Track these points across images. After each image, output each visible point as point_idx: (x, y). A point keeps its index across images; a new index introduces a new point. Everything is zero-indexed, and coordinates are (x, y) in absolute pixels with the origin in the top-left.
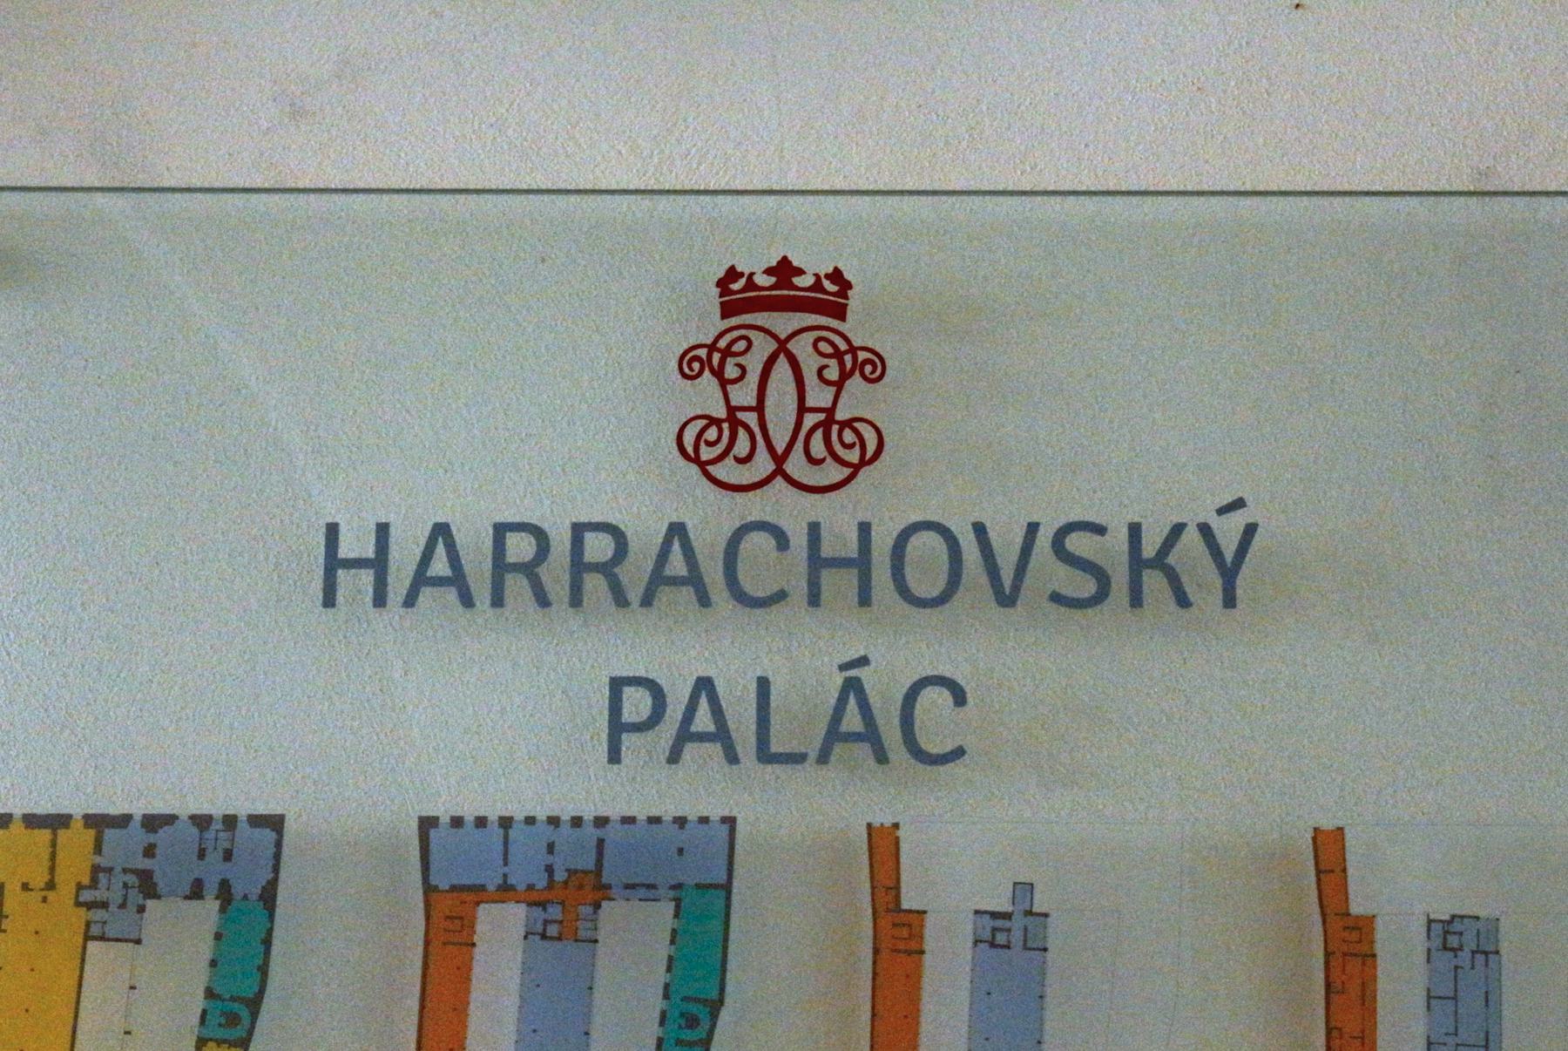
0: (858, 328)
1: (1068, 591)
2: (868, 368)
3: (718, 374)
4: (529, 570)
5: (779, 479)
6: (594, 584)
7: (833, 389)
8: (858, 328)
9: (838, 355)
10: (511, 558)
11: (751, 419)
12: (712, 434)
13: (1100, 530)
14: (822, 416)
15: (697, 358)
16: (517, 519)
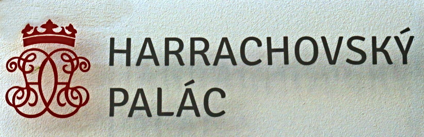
0: (78, 49)
1: (353, 59)
2: (83, 66)
3: (23, 69)
4: (176, 53)
5: (47, 113)
7: (69, 75)
9: (71, 60)
10: (171, 49)
11: (36, 88)
12: (20, 94)
13: (363, 39)
14: (64, 86)
15: (14, 63)
16: (173, 37)
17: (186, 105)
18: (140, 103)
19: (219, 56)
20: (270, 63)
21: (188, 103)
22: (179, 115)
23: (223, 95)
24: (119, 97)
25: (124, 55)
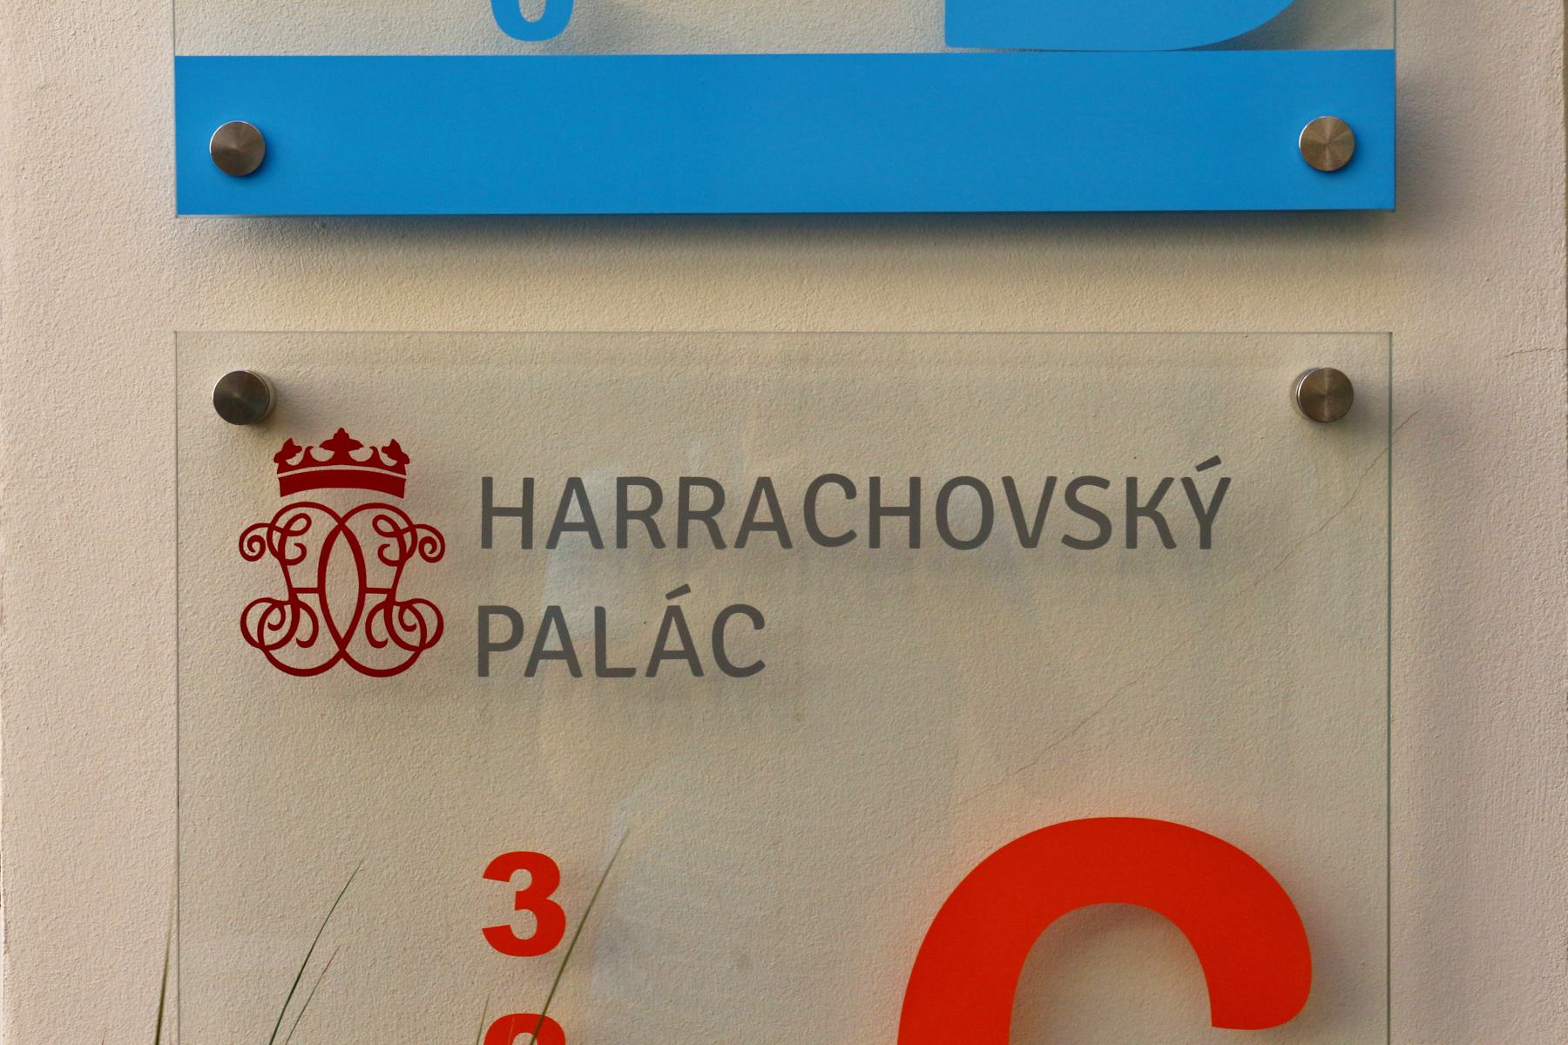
0: (416, 506)
1: (1077, 536)
2: (428, 547)
3: (279, 554)
4: (646, 516)
5: (342, 662)
6: (697, 528)
8: (416, 506)
9: (398, 533)
11: (312, 600)
12: (275, 617)
13: (1103, 483)
15: (257, 538)
17: (547, 647)
18: (553, 643)
19: (749, 524)
20: (875, 542)
21: (674, 642)
22: (652, 671)
23: (759, 621)
24: (500, 629)
25: (906, 520)
